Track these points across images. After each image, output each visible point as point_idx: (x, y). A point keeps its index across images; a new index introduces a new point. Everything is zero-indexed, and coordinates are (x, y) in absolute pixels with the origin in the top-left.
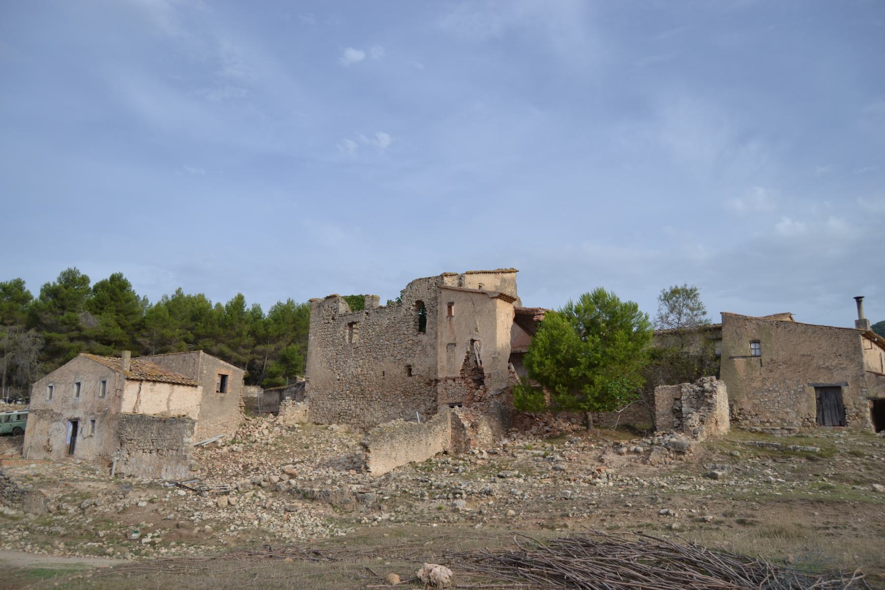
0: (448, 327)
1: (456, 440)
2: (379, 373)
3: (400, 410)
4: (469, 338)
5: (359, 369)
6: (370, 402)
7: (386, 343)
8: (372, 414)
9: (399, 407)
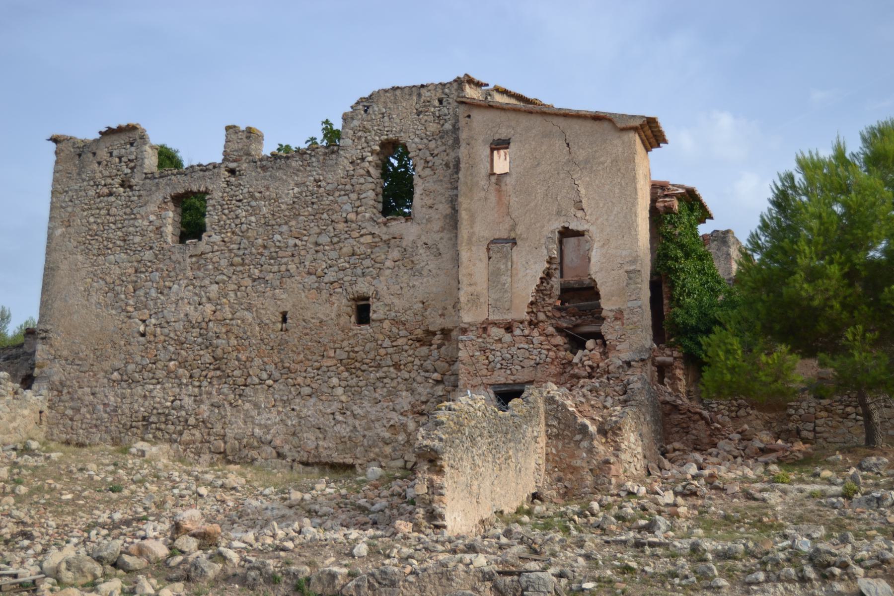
0: (493, 198)
1: (560, 467)
2: (271, 315)
3: (336, 406)
4: (557, 225)
5: (209, 308)
6: (240, 389)
7: (292, 242)
8: (248, 419)
9: (333, 397)
